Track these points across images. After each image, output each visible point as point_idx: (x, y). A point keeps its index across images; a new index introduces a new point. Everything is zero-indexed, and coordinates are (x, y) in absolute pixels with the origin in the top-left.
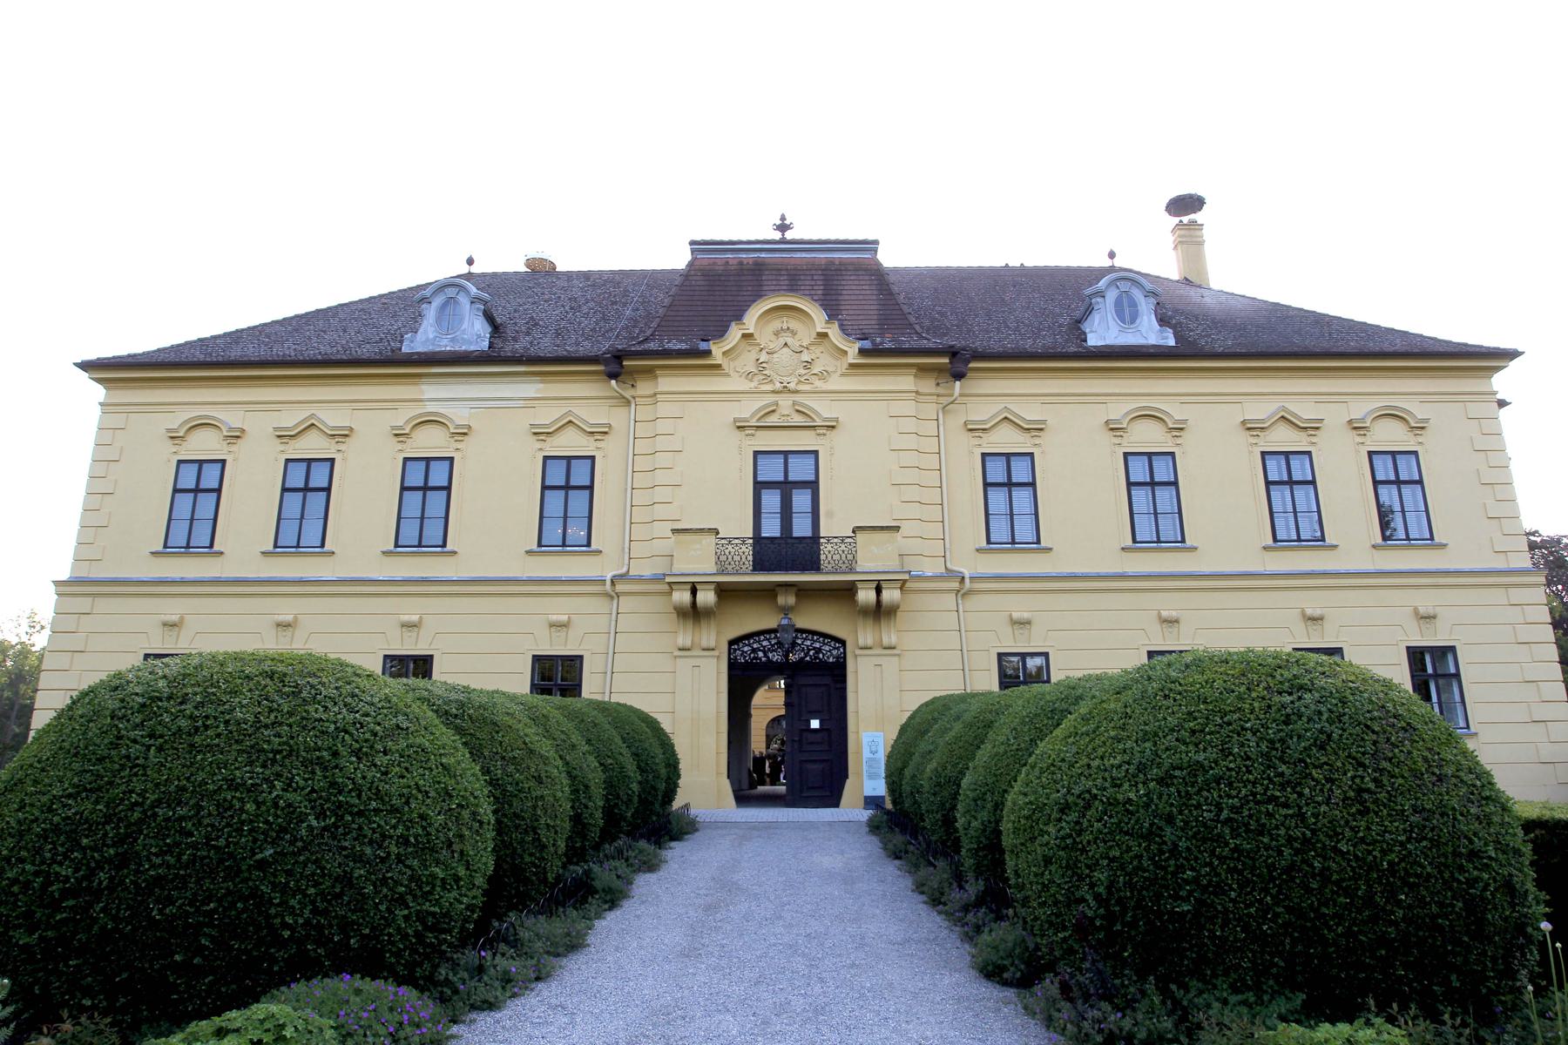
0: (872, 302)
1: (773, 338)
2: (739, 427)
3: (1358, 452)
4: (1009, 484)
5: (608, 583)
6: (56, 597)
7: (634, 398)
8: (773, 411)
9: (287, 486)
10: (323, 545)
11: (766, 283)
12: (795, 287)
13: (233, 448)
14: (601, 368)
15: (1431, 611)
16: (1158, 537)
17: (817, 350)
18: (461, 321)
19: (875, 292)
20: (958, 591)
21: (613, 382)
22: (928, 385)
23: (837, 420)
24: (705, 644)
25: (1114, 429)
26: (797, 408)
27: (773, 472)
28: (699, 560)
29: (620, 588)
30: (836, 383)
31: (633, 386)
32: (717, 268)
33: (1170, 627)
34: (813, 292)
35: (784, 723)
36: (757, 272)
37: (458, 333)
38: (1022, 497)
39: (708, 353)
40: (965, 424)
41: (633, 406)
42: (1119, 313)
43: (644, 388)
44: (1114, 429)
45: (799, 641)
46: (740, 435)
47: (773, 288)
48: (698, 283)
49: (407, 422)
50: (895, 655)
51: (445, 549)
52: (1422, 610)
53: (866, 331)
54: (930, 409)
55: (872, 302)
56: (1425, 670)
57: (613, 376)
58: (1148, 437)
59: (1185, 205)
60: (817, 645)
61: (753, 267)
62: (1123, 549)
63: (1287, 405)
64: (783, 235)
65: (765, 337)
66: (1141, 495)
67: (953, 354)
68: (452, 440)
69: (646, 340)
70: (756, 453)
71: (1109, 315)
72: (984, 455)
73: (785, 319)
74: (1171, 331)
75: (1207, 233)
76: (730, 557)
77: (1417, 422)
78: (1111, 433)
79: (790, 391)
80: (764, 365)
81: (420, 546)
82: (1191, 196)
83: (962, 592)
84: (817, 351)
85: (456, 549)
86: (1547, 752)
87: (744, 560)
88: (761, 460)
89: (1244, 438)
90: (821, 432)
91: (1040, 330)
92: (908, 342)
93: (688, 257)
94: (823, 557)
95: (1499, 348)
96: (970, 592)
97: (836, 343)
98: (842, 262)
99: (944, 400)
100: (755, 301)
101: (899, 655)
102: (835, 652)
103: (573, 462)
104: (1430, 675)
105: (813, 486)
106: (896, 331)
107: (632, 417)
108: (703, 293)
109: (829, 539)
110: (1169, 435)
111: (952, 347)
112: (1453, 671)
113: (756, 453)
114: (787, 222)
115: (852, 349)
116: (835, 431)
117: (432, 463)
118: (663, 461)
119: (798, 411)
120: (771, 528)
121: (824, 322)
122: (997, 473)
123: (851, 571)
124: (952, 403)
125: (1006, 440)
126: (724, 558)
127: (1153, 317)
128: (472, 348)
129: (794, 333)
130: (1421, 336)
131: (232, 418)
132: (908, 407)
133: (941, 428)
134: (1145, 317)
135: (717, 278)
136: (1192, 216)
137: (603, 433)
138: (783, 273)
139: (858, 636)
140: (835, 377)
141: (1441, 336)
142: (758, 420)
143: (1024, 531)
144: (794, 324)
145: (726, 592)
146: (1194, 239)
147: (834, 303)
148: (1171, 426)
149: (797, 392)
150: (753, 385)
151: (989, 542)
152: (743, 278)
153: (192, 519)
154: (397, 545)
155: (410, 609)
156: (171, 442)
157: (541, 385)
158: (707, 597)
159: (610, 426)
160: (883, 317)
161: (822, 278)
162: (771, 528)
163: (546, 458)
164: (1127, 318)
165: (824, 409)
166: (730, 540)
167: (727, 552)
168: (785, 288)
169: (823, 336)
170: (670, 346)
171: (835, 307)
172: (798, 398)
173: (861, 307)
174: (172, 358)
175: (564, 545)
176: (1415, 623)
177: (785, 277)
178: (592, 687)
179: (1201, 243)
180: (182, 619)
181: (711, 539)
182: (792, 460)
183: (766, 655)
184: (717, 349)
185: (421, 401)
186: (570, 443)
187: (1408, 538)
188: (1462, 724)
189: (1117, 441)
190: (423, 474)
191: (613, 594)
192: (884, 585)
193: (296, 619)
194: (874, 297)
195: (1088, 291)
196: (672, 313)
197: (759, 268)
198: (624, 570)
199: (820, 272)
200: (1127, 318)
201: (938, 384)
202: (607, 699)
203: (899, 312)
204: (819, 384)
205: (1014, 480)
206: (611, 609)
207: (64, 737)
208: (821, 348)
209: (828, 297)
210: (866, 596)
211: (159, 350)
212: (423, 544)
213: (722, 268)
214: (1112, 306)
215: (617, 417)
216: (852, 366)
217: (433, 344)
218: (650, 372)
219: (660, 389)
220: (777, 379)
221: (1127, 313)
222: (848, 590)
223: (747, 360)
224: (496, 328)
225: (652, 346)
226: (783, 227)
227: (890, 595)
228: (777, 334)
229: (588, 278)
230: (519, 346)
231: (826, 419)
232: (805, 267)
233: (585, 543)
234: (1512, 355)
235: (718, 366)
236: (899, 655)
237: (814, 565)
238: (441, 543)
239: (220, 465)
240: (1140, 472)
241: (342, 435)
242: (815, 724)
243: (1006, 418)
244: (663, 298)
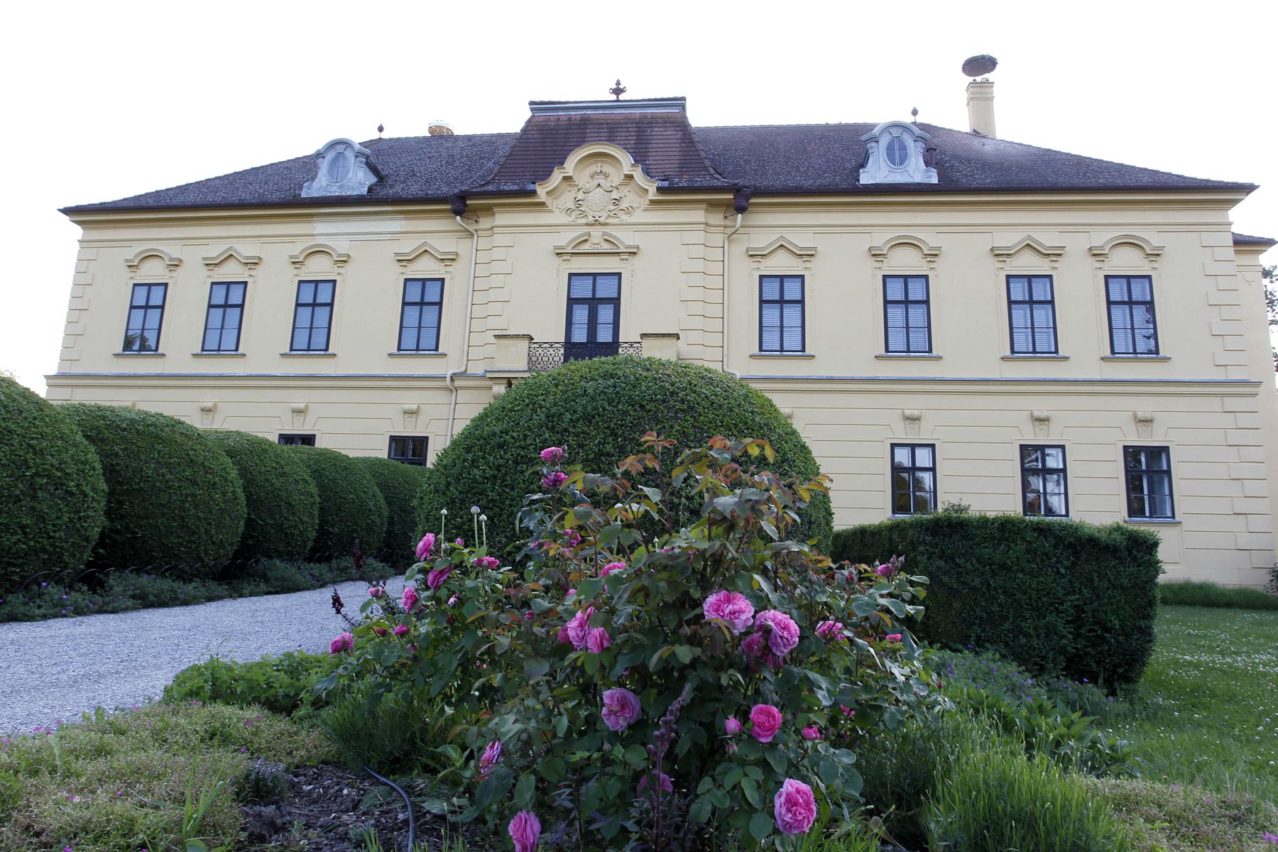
0: (675, 149)
1: (589, 180)
2: (558, 254)
3: (1095, 275)
4: (906, 302)
5: (448, 379)
6: (47, 387)
7: (476, 231)
8: (586, 240)
9: (212, 303)
10: (237, 349)
11: (589, 135)
12: (613, 138)
13: (174, 274)
14: (449, 207)
15: (1148, 416)
17: (624, 191)
18: (347, 173)
19: (679, 141)
21: (458, 218)
22: (717, 218)
23: (939, 248)
25: (876, 255)
26: (605, 237)
27: (583, 290)
29: (457, 383)
30: (640, 216)
32: (550, 123)
33: (912, 424)
34: (627, 142)
36: (583, 126)
37: (345, 181)
38: (792, 313)
39: (533, 193)
43: (485, 223)
44: (876, 255)
46: (558, 260)
47: (594, 139)
48: (534, 136)
51: (327, 353)
52: (1140, 415)
53: (668, 173)
54: (718, 239)
55: (675, 149)
57: (458, 212)
58: (905, 262)
59: (979, 65)
61: (578, 122)
62: (876, 357)
63: (1032, 234)
65: (583, 179)
66: (897, 313)
67: (736, 190)
68: (335, 266)
69: (487, 183)
70: (571, 275)
71: (881, 157)
72: (1008, 277)
73: (599, 164)
74: (935, 170)
75: (997, 91)
76: (540, 358)
77: (1152, 250)
78: (1094, 258)
79: (601, 224)
80: (580, 202)
81: (309, 350)
82: (983, 57)
86: (1244, 540)
88: (575, 281)
89: (993, 263)
91: (825, 172)
92: (699, 181)
93: (529, 114)
95: (1237, 183)
98: (653, 117)
99: (729, 231)
100: (571, 151)
104: (1144, 471)
105: (616, 302)
106: (692, 173)
107: (475, 247)
108: (538, 145)
110: (925, 260)
111: (736, 184)
112: (1165, 468)
113: (571, 275)
114: (621, 87)
115: (652, 188)
116: (636, 258)
117: (320, 285)
118: (495, 280)
119: (606, 240)
120: (580, 336)
121: (630, 165)
122: (772, 292)
124: (734, 233)
125: (781, 264)
127: (921, 160)
128: (355, 193)
129: (606, 176)
130: (1170, 174)
131: (173, 251)
132: (699, 237)
134: (913, 160)
135: (549, 132)
136: (986, 76)
137: (449, 259)
138: (604, 126)
141: (1187, 174)
143: (792, 341)
144: (607, 168)
146: (985, 96)
147: (643, 150)
148: (926, 252)
149: (606, 224)
150: (570, 219)
151: (761, 350)
152: (571, 131)
153: (311, 328)
154: (291, 350)
155: (299, 398)
156: (128, 269)
159: (457, 254)
160: (683, 161)
161: (635, 130)
162: (580, 336)
163: (406, 280)
164: (897, 160)
165: (627, 238)
166: (540, 344)
167: (537, 354)
168: (604, 138)
169: (629, 177)
170: (506, 188)
171: (644, 154)
172: (606, 229)
173: (666, 154)
174: (151, 202)
175: (418, 349)
176: (902, 423)
177: (605, 130)
179: (991, 99)
180: (215, 406)
182: (599, 280)
184: (542, 190)
185: (313, 235)
186: (426, 268)
187: (1135, 352)
188: (1169, 514)
189: (878, 265)
190: (313, 293)
191: (452, 388)
193: (307, 407)
194: (678, 145)
195: (863, 138)
196: (511, 162)
197: (584, 123)
198: (463, 369)
199: (634, 125)
200: (897, 160)
201: (726, 217)
203: (698, 157)
204: (625, 218)
205: (786, 298)
206: (451, 401)
207: (178, 492)
208: (629, 188)
209: (639, 146)
211: (124, 200)
212: (311, 348)
213: (553, 123)
214: (885, 152)
215: (463, 247)
216: (653, 202)
217: (325, 191)
218: (489, 210)
219: (497, 222)
220: (590, 214)
221: (897, 155)
223: (567, 199)
224: (381, 178)
225: (490, 188)
226: (618, 91)
228: (592, 177)
229: (469, 138)
230: (398, 189)
231: (628, 247)
232: (622, 121)
233: (434, 348)
234: (1248, 189)
235: (543, 204)
238: (324, 348)
239: (163, 287)
240: (896, 292)
241: (254, 263)
243: (1028, 245)
244: (507, 150)
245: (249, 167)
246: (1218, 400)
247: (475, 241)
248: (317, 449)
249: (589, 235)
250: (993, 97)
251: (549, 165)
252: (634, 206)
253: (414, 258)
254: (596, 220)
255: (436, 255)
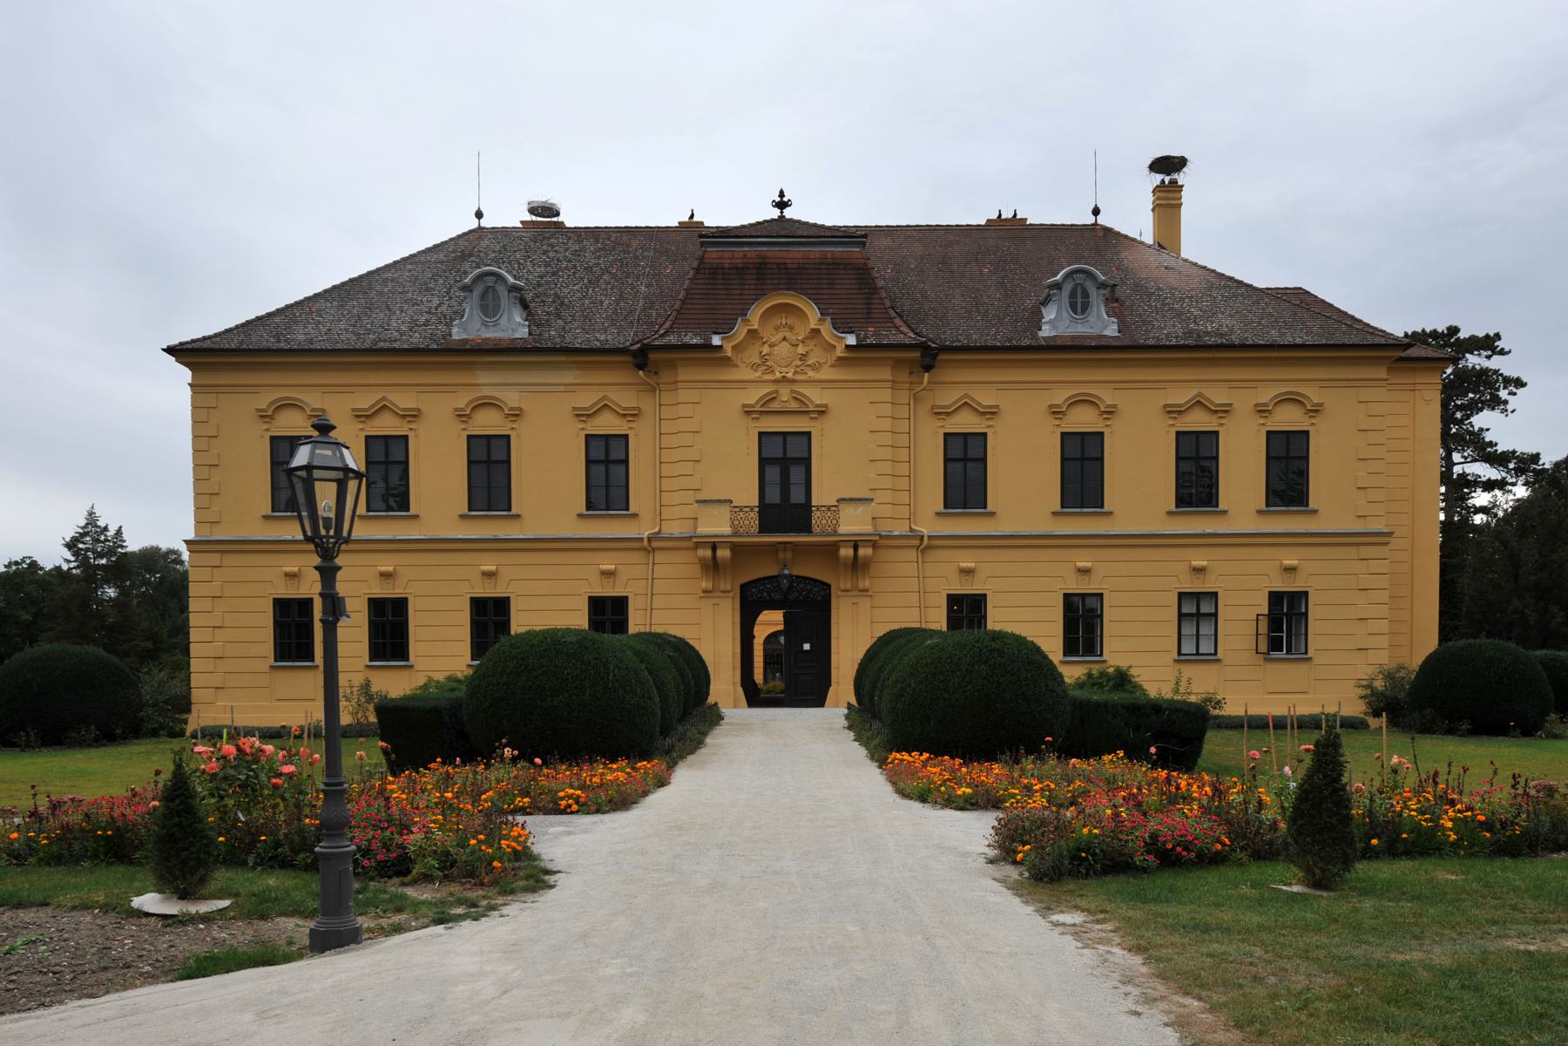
2: (746, 412)
5: (646, 541)
8: (774, 398)
16: (785, 442)
17: (811, 344)
20: (919, 547)
21: (641, 373)
22: (904, 376)
24: (722, 587)
26: (794, 395)
28: (717, 525)
29: (654, 544)
30: (827, 373)
31: (656, 373)
32: (724, 261)
35: (782, 639)
40: (933, 407)
41: (657, 392)
42: (1073, 307)
45: (795, 585)
49: (467, 405)
50: (867, 596)
51: (511, 513)
54: (904, 396)
56: (1283, 610)
57: (640, 367)
59: (1168, 165)
60: (809, 587)
64: (782, 212)
65: (769, 334)
67: (924, 347)
77: (1312, 406)
83: (922, 547)
84: (811, 344)
85: (520, 513)
87: (752, 523)
90: (813, 416)
94: (814, 522)
96: (928, 547)
97: (827, 338)
101: (871, 596)
102: (822, 593)
103: (789, 439)
105: (806, 462)
107: (657, 402)
109: (818, 508)
110: (1101, 418)
114: (785, 199)
120: (774, 497)
123: (835, 533)
125: (965, 423)
126: (736, 522)
129: (791, 328)
132: (886, 394)
133: (912, 411)
134: (1095, 309)
136: (1175, 176)
137: (633, 415)
139: (839, 584)
140: (826, 368)
142: (762, 406)
145: (736, 549)
150: (758, 374)
157: (579, 372)
158: (724, 553)
159: (639, 409)
165: (816, 396)
166: (741, 509)
167: (739, 517)
169: (816, 332)
173: (849, 301)
178: (520, 623)
181: (726, 510)
183: (769, 595)
185: (477, 385)
186: (607, 424)
192: (859, 543)
198: (657, 530)
201: (911, 373)
202: (648, 630)
210: (846, 552)
215: (646, 403)
216: (840, 359)
218: (672, 365)
222: (833, 548)
226: (782, 205)
227: (864, 552)
228: (777, 329)
231: (817, 406)
235: (729, 359)
236: (871, 596)
237: (807, 528)
241: (413, 416)
242: (807, 647)
245: (346, 279)
246: (1354, 549)
247: (657, 396)
248: (518, 636)
249: (776, 392)
250: (1181, 204)
251: (733, 317)
252: (821, 361)
253: (596, 411)
254: (784, 377)
255: (618, 410)
